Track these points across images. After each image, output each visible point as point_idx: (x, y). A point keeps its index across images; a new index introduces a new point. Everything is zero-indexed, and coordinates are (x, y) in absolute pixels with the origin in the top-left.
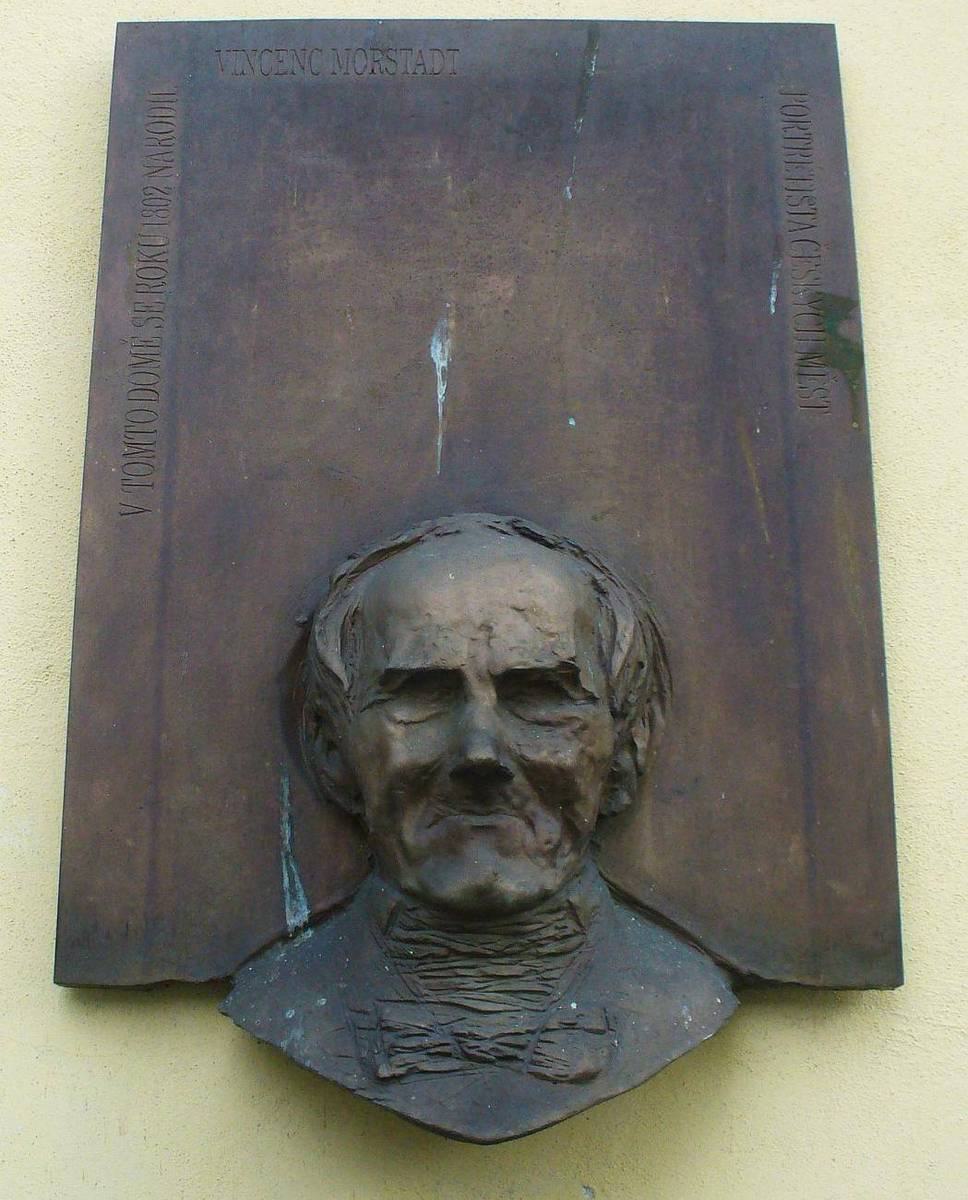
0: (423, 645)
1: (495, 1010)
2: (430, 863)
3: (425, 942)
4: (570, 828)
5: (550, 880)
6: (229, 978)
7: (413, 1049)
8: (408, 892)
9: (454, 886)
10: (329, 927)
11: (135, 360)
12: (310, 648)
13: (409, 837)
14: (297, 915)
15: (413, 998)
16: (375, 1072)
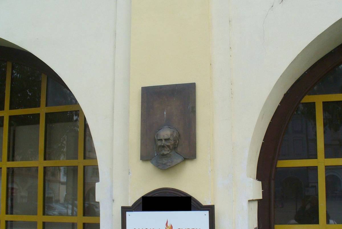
1: (165, 161)
4: (170, 149)
5: (168, 152)
9: (162, 153)
14: (156, 155)
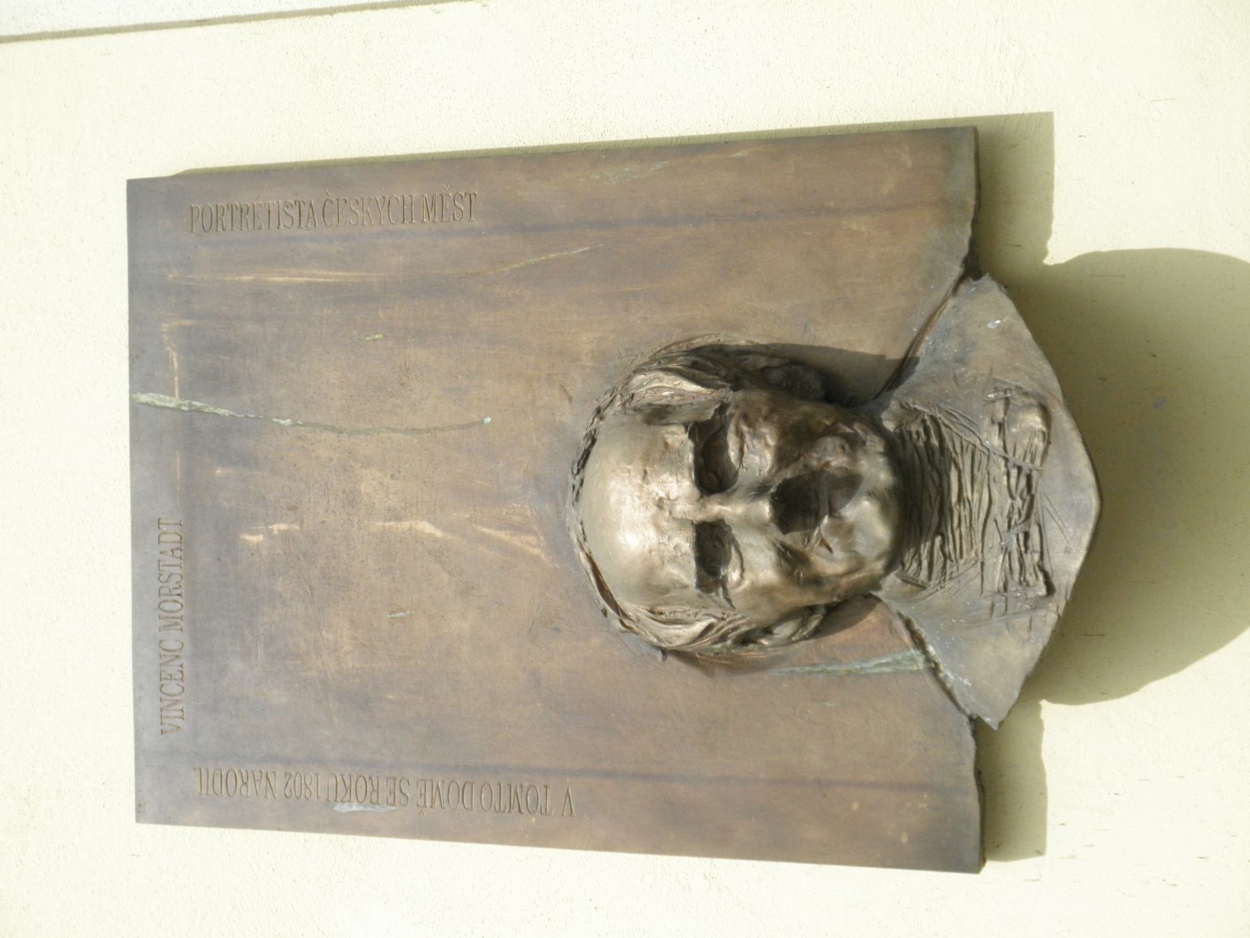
0: (676, 557)
2: (860, 549)
3: (931, 553)
6: (971, 719)
7: (1022, 565)
8: (888, 568)
10: (924, 634)
11: (437, 803)
12: (685, 649)
13: (839, 568)
15: (979, 564)
16: (1042, 598)
